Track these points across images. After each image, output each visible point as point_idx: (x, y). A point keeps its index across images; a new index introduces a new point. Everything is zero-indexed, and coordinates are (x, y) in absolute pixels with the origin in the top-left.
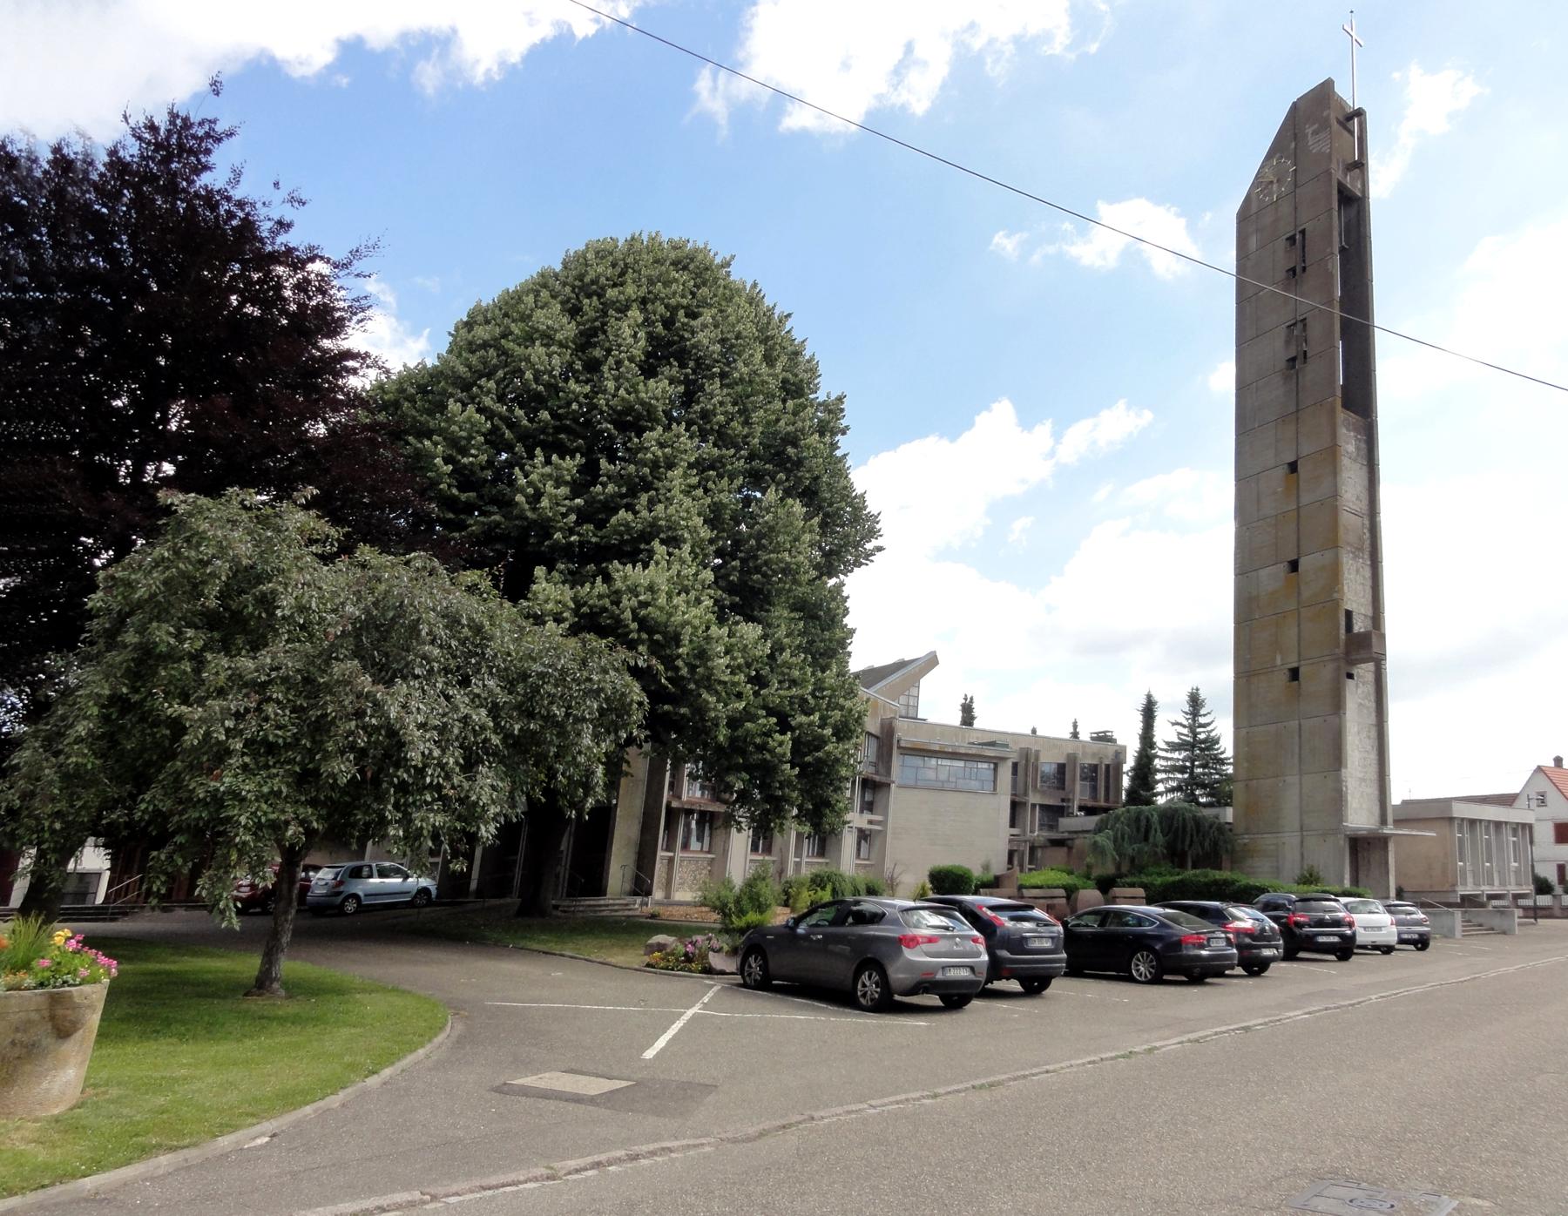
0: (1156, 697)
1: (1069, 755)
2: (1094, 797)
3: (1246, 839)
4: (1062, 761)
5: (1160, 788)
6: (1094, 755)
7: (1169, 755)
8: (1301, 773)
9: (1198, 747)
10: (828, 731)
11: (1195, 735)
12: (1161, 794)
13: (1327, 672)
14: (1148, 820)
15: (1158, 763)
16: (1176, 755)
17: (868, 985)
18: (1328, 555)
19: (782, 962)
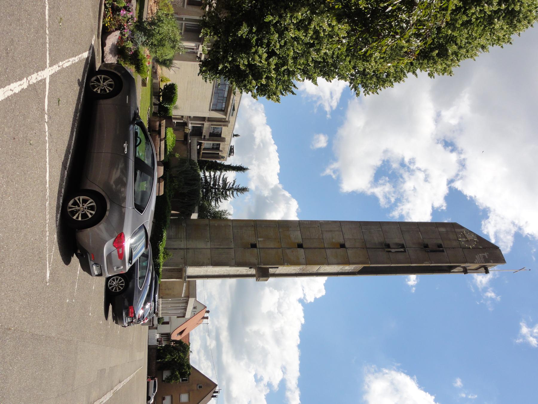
0: (247, 172)
1: (224, 138)
2: (204, 149)
3: (184, 225)
4: (222, 136)
5: (207, 174)
6: (224, 148)
7: (221, 179)
8: (211, 249)
9: (225, 191)
10: (264, 82)
11: (229, 190)
12: (204, 172)
13: (254, 260)
14: (194, 184)
15: (218, 173)
16: (221, 182)
17: (84, 207)
18: (304, 261)
19: (107, 109)
